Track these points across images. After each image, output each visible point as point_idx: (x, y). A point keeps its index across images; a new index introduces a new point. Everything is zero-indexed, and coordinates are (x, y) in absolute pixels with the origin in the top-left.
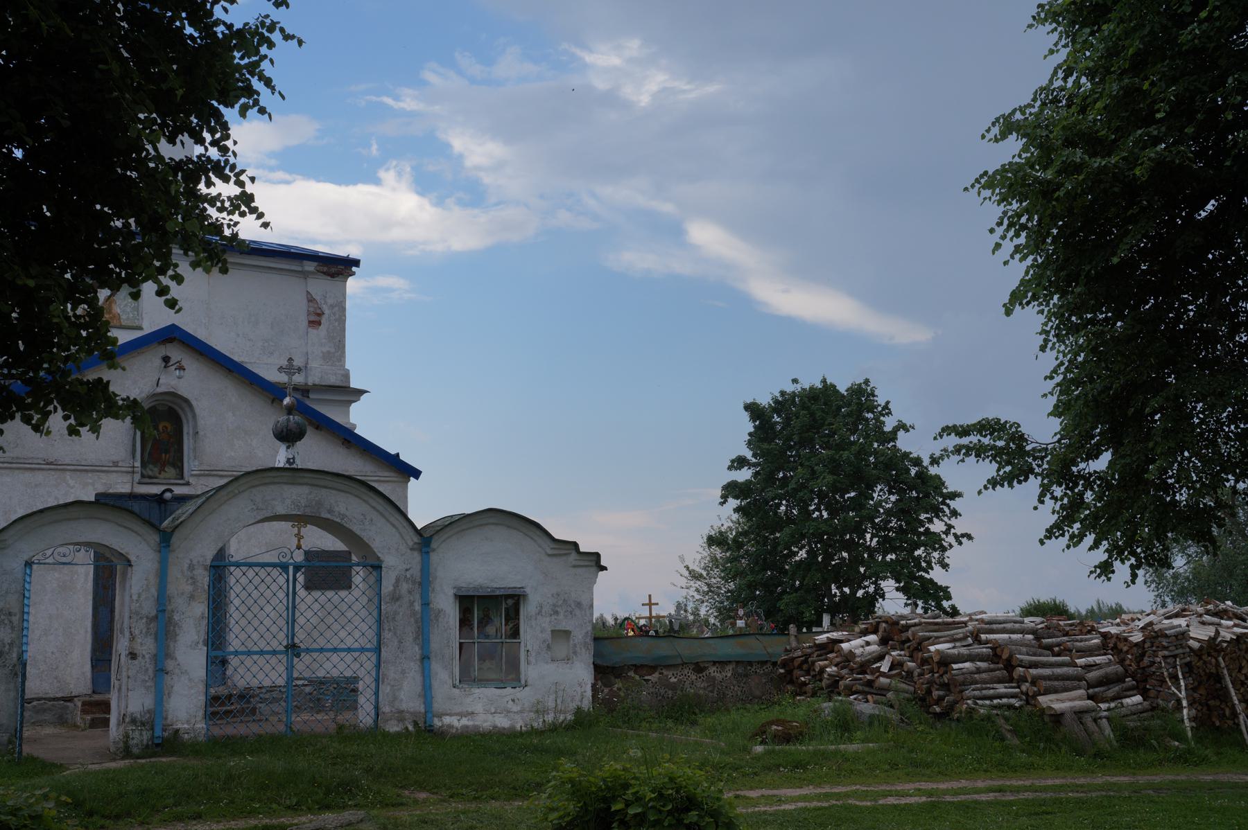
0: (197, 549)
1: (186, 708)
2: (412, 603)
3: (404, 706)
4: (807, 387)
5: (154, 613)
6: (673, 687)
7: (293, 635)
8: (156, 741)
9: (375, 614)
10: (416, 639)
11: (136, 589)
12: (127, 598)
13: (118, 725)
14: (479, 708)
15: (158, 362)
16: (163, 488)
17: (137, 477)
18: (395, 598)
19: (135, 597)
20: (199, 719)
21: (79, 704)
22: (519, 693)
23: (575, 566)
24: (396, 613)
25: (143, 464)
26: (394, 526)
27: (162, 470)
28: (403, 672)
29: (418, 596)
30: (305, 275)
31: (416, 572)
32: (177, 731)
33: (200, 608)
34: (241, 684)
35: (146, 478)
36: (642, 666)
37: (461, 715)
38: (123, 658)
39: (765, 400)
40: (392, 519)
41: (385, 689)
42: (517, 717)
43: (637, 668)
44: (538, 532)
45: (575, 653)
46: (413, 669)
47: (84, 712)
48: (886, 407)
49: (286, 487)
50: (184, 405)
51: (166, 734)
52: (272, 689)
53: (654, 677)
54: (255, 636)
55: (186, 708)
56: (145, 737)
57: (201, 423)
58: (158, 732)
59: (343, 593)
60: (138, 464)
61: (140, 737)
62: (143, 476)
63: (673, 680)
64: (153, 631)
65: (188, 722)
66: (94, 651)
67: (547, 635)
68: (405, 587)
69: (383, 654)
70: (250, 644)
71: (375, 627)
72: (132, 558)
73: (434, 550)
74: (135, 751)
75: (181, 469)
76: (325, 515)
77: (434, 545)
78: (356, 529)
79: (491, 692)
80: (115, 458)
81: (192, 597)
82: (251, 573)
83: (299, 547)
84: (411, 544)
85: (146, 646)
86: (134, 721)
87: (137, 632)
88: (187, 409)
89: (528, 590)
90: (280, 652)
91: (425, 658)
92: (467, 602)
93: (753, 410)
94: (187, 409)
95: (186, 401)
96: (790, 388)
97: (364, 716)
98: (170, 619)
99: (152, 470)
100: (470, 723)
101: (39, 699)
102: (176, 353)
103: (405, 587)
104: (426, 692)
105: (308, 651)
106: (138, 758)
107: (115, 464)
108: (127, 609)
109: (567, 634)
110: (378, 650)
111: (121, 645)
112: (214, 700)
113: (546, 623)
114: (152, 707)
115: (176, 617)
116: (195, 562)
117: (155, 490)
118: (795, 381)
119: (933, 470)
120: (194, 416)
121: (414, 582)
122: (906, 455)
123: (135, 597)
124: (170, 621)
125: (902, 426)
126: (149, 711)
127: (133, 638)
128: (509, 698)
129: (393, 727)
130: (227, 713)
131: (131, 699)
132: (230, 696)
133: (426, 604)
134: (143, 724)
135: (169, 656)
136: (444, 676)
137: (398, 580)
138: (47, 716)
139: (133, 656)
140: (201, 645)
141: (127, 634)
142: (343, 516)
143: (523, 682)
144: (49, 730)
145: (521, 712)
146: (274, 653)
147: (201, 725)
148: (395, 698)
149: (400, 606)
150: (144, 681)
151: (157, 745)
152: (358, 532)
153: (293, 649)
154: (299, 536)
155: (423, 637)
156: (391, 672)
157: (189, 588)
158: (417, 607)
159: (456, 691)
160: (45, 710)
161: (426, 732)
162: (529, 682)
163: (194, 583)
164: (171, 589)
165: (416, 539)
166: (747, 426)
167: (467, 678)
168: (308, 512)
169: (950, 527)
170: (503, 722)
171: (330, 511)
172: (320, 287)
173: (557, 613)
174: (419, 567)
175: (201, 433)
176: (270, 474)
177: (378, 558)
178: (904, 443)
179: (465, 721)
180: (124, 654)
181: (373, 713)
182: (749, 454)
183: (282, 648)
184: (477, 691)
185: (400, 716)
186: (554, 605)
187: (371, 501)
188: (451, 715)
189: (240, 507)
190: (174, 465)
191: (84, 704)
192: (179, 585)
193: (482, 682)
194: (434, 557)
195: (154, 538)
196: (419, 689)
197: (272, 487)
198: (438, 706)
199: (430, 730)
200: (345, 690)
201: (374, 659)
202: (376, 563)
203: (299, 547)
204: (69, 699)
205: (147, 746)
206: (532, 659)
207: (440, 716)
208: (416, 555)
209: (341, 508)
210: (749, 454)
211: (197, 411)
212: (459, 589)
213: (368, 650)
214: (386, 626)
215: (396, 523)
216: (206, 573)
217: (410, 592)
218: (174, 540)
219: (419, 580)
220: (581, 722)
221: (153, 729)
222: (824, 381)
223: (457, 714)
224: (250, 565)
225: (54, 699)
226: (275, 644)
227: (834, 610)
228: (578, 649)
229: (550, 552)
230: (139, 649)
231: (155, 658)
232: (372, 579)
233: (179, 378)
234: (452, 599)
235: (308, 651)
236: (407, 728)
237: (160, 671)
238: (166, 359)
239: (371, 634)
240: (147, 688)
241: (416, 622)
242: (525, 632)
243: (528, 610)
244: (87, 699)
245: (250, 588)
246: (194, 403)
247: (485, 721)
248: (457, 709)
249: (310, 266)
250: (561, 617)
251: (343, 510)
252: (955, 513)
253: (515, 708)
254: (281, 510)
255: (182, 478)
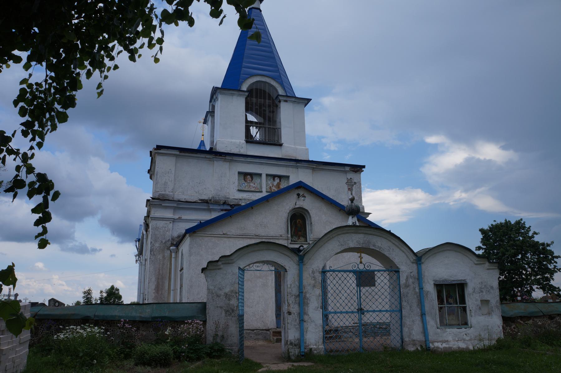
0: (315, 263)
1: (314, 338)
2: (414, 289)
3: (415, 338)
4: (499, 223)
5: (298, 293)
6: (540, 327)
7: (361, 304)
8: (302, 354)
9: (398, 293)
10: (418, 305)
11: (291, 278)
12: (286, 287)
13: (285, 345)
14: (450, 338)
15: (296, 196)
16: (299, 245)
17: (290, 241)
18: (407, 286)
19: (289, 286)
20: (320, 343)
21: (272, 332)
22: (470, 331)
23: (488, 269)
24: (408, 293)
25: (292, 236)
26: (403, 252)
27: (299, 238)
28: (413, 321)
29: (417, 285)
30: (346, 172)
31: (415, 273)
32: (311, 349)
33: (318, 291)
34: (336, 324)
35: (293, 242)
36: (525, 317)
37: (443, 342)
38: (285, 314)
39: (486, 227)
40: (402, 249)
41: (405, 330)
42: (469, 343)
43: (521, 318)
44: (470, 253)
45: (492, 311)
46: (418, 319)
47: (274, 335)
48: (529, 228)
49: (353, 235)
50: (306, 213)
51: (306, 350)
52: (347, 327)
53: (531, 322)
54: (338, 305)
55: (314, 338)
56: (297, 352)
57: (313, 219)
58: (302, 350)
59: (373, 288)
60: (290, 236)
61: (294, 351)
62: (292, 241)
63: (540, 323)
64: (297, 302)
65: (316, 345)
66: (276, 311)
67: (479, 303)
68: (411, 281)
69: (403, 313)
70: (336, 308)
71: (398, 300)
72: (287, 268)
73: (423, 263)
74: (293, 358)
75: (306, 238)
76: (372, 247)
77: (423, 261)
78: (386, 253)
79: (455, 330)
80: (281, 234)
81: (314, 286)
82: (340, 275)
83: (361, 263)
84: (412, 260)
85: (295, 309)
86: (291, 344)
87: (291, 302)
88: (307, 214)
89: (468, 281)
90: (355, 312)
91: (423, 315)
92: (440, 287)
93: (482, 231)
94: (307, 214)
95: (307, 211)
96: (494, 223)
97: (394, 341)
98: (305, 296)
99: (295, 238)
100: (447, 346)
101: (257, 330)
102: (301, 192)
103: (411, 281)
104: (425, 331)
105: (368, 311)
106: (294, 362)
107: (281, 236)
108: (286, 291)
109: (487, 302)
110: (401, 311)
111: (285, 308)
112: (326, 332)
113: (478, 297)
114: (299, 337)
115: (308, 296)
116: (315, 270)
117: (297, 246)
118: (495, 221)
119: (548, 248)
120: (310, 217)
121: (415, 278)
122: (538, 242)
123: (289, 286)
124: (305, 297)
125: (535, 233)
126: (298, 339)
127: (289, 305)
128: (464, 333)
129: (411, 349)
130: (331, 337)
131: (292, 335)
132: (330, 331)
133: (421, 288)
134: (295, 345)
135: (306, 313)
136: (432, 323)
137: (407, 277)
138: (260, 337)
139: (289, 313)
140: (319, 309)
141: (286, 303)
142: (380, 248)
143: (470, 325)
144: (261, 343)
145: (470, 340)
146: (335, 313)
147: (322, 347)
148: (410, 334)
149: (409, 290)
150: (295, 325)
151: (303, 356)
152: (387, 255)
153: (361, 311)
154: (361, 257)
155: (421, 304)
156: (407, 321)
157: (313, 282)
158: (417, 290)
159: (439, 330)
160: (259, 334)
161: (426, 351)
162: (473, 325)
163: (315, 280)
164: (305, 282)
165: (414, 258)
166: (481, 236)
167: (443, 324)
168: (364, 246)
169: (555, 266)
170: (462, 345)
171: (374, 246)
172: (351, 175)
173: (482, 292)
174: (416, 271)
175: (313, 223)
176: (346, 229)
177: (397, 267)
178: (536, 239)
179: (444, 345)
180: (286, 312)
181: (400, 341)
182: (481, 245)
183: (356, 310)
184: (448, 330)
185: (414, 342)
186: (481, 288)
187: (392, 240)
188: (438, 342)
189: (334, 245)
190: (303, 237)
191: (274, 332)
192: (307, 280)
193: (451, 326)
194: (423, 267)
195: (296, 259)
196: (421, 330)
197: (347, 235)
198: (431, 337)
199: (428, 349)
200: (382, 329)
201: (399, 315)
202: (397, 270)
203: (361, 263)
204: (268, 330)
205: (298, 355)
206: (473, 314)
207: (433, 343)
208: (415, 265)
209: (379, 244)
210: (481, 245)
211: (311, 215)
212: (435, 281)
213: (396, 311)
214: (403, 299)
215: (404, 250)
216: (320, 275)
217: (413, 283)
218: (305, 259)
219: (417, 277)
220: (500, 346)
221: (300, 347)
222: (506, 220)
223: (440, 342)
224: (339, 271)
225: (263, 330)
226: (352, 308)
227: (81, 326)
228: (494, 309)
229: (476, 263)
230: (292, 310)
231: (299, 314)
232: (395, 277)
233: (304, 200)
234: (433, 286)
235: (368, 311)
236: (417, 349)
237: (302, 321)
238: (298, 195)
239: (396, 303)
240: (296, 328)
241: (417, 297)
242: (468, 301)
243: (468, 291)
244: (274, 330)
245: (337, 285)
246: (310, 212)
247: (454, 345)
248: (441, 339)
249: (348, 169)
250: (484, 293)
251: (380, 245)
252: (556, 263)
253: (467, 338)
254: (352, 245)
255: (307, 241)
